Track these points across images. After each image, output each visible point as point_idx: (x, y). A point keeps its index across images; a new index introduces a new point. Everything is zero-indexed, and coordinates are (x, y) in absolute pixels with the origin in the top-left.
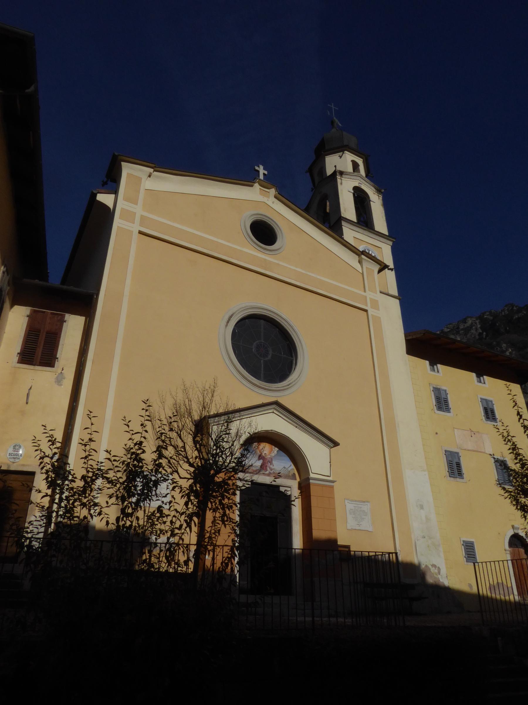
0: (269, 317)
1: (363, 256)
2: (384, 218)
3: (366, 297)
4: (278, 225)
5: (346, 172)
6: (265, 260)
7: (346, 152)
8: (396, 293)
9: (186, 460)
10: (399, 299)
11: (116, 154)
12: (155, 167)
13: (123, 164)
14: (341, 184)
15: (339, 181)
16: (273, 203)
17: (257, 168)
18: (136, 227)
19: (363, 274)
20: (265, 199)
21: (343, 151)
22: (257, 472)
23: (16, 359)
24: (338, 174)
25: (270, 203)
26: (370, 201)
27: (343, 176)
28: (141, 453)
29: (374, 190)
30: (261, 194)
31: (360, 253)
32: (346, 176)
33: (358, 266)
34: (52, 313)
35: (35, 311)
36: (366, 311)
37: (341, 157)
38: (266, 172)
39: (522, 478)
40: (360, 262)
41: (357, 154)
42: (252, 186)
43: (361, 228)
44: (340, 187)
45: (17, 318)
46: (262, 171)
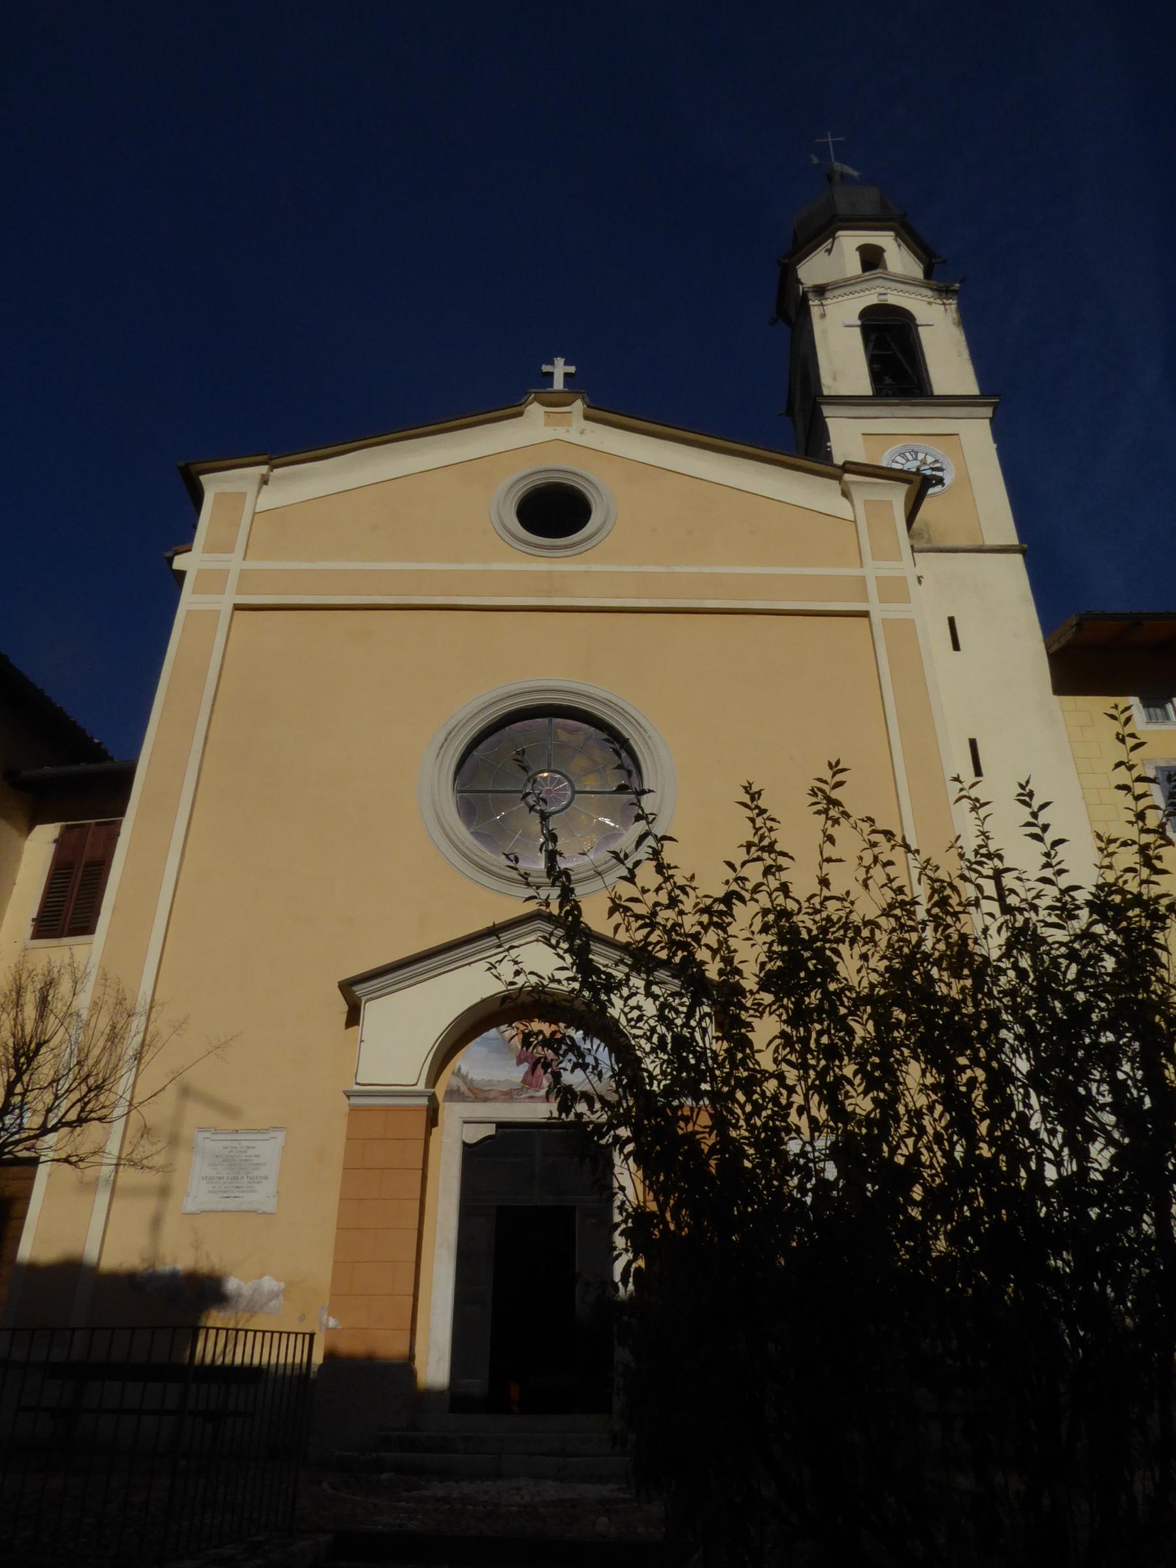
0: (560, 706)
1: (848, 477)
2: (966, 354)
3: (863, 580)
4: (587, 480)
5: (835, 283)
6: (550, 573)
7: (840, 233)
8: (1013, 539)
9: (74, 1159)
10: (1023, 552)
11: (182, 464)
12: (271, 459)
13: (203, 478)
14: (823, 316)
15: (815, 311)
16: (582, 433)
17: (546, 368)
18: (225, 603)
19: (855, 522)
20: (559, 433)
21: (832, 235)
22: (510, 1095)
23: (29, 930)
24: (810, 296)
25: (573, 436)
26: (917, 326)
27: (828, 294)
28: (960, 896)
29: (930, 293)
30: (547, 424)
31: (838, 471)
32: (837, 292)
33: (841, 507)
34: (97, 824)
35: (68, 827)
36: (865, 614)
37: (829, 251)
38: (572, 369)
39: (935, 1222)
40: (846, 494)
41: (877, 224)
42: (521, 414)
43: (905, 405)
44: (818, 326)
45: (39, 847)
46: (560, 369)
